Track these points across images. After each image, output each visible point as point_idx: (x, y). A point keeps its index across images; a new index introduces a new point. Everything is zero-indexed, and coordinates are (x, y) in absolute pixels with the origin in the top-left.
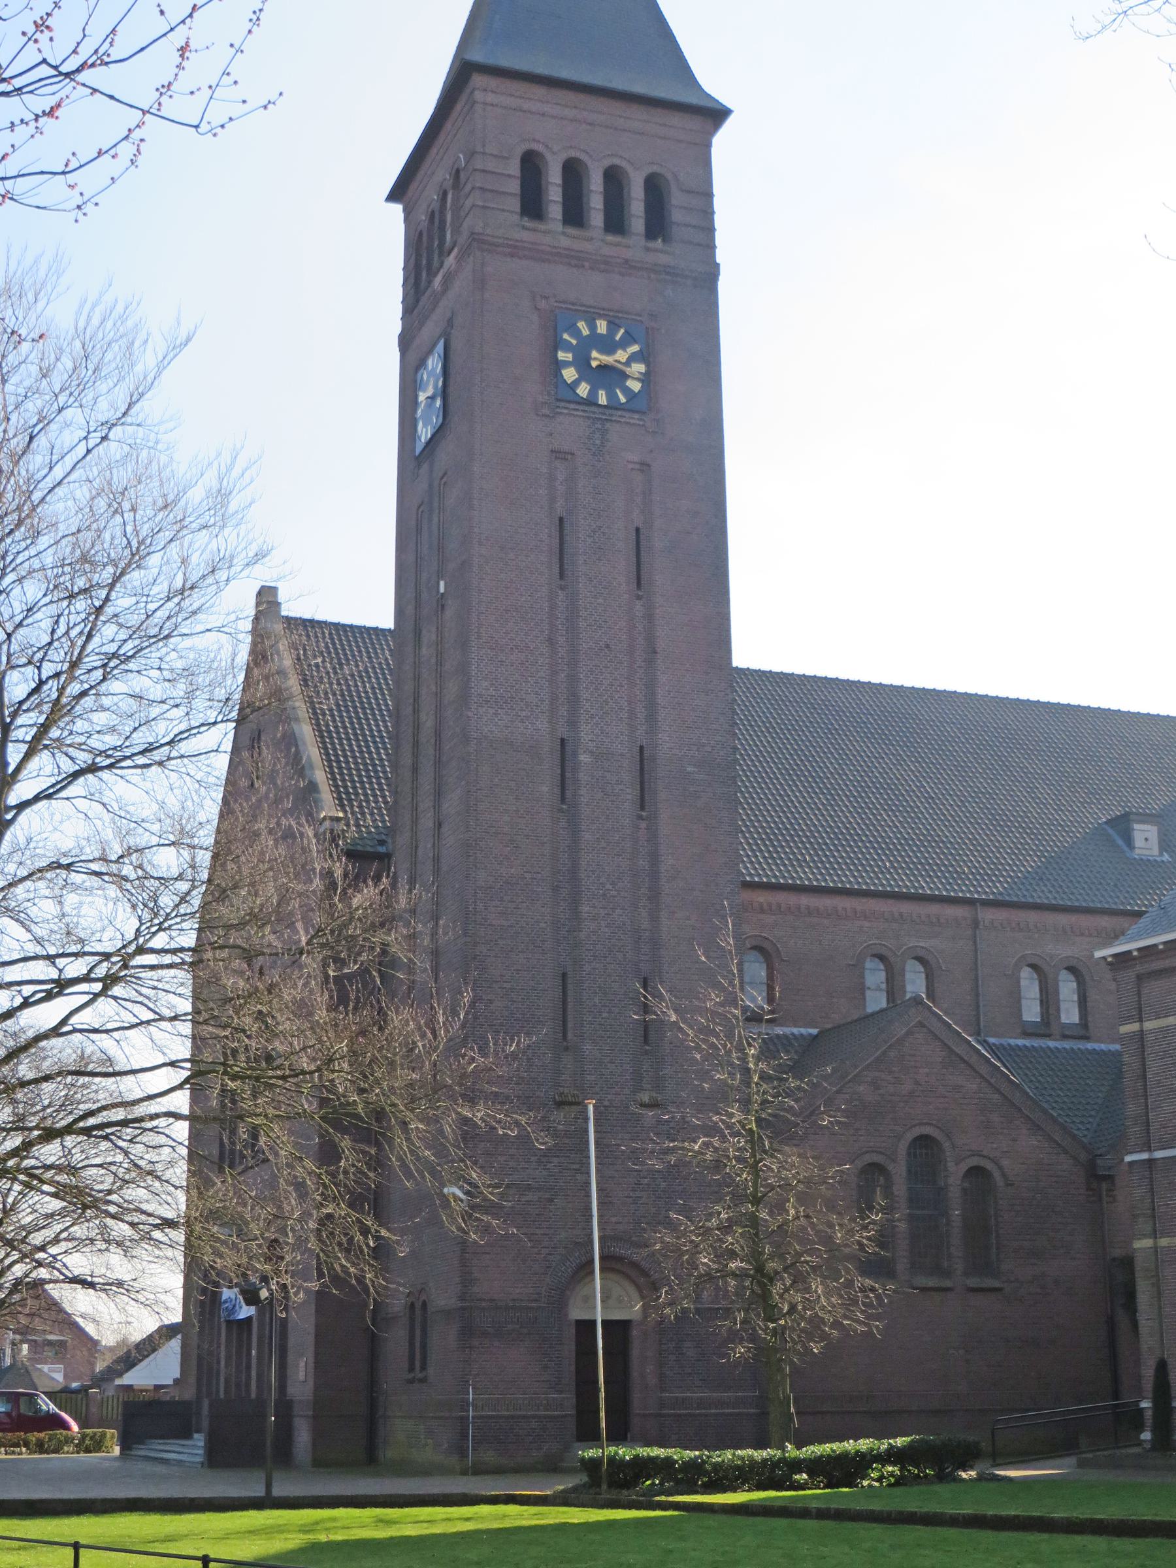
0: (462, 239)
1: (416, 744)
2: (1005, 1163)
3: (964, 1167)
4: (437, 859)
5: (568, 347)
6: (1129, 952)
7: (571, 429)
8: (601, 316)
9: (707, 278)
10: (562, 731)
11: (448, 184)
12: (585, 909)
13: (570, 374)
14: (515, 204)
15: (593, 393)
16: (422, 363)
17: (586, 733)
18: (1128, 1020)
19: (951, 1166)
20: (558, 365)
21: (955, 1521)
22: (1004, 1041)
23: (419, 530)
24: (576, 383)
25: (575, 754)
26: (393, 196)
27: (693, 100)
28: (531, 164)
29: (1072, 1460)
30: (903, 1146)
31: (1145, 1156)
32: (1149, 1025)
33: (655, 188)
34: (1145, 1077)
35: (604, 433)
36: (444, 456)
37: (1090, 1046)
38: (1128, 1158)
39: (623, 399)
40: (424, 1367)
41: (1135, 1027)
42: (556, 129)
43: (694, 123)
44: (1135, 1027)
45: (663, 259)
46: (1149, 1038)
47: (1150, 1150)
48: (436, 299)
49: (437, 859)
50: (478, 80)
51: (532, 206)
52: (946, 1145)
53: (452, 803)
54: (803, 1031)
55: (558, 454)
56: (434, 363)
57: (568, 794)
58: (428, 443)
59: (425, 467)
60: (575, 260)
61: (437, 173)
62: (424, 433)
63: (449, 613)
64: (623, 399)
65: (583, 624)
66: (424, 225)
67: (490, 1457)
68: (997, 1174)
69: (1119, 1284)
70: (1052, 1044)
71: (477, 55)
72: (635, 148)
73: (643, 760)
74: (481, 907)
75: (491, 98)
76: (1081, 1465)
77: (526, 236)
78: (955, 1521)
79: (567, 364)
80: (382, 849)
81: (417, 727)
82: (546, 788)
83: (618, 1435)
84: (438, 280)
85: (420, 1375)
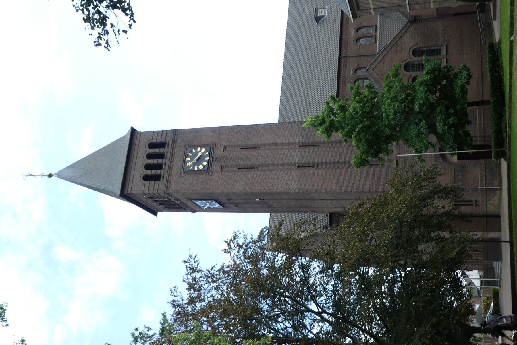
0: (166, 196)
1: (300, 206)
2: (411, 46)
3: (412, 57)
4: (331, 200)
5: (194, 168)
6: (352, 13)
7: (216, 167)
8: (185, 159)
9: (175, 132)
10: (295, 167)
11: (152, 200)
12: (343, 160)
13: (201, 167)
14: (157, 182)
15: (205, 161)
16: (199, 206)
17: (296, 161)
18: (370, 13)
19: (412, 60)
20: (199, 170)
21: (512, 11)
22: (378, 47)
23: (243, 207)
24: (203, 165)
25: (302, 163)
26: (156, 215)
27: (129, 136)
28: (146, 178)
29: (494, 22)
30: (406, 73)
31: (408, 6)
32: (372, 7)
33: (152, 146)
34: (386, 7)
35: (216, 158)
36: (223, 200)
37: (378, 25)
38: (408, 11)
39: (207, 153)
40: (472, 201)
41: (372, 10)
42: (138, 171)
43: (136, 141)
44: (372, 10)
45: (170, 143)
46: (375, 7)
47: (406, 5)
48: (182, 203)
49: (331, 200)
50: (125, 192)
51: (157, 178)
52: (406, 61)
53: (316, 196)
54: (379, 19)
55: (222, 169)
56: (199, 203)
57: (312, 165)
58: (220, 204)
59: (226, 205)
60: (171, 166)
61: (150, 202)
62: (217, 205)
63: (264, 198)
64: (207, 153)
65: (267, 162)
66: (163, 206)
67: (496, 183)
68: (414, 48)
69: (442, 14)
70: (378, 35)
71: (118, 192)
72: (142, 150)
73: (302, 146)
74: (343, 188)
75: (130, 189)
76: (495, 19)
77: (165, 179)
78: (512, 11)
79: (198, 168)
80: (329, 215)
81: (295, 206)
82: (311, 171)
83: (490, 147)
84: (177, 202)
85: (474, 202)
